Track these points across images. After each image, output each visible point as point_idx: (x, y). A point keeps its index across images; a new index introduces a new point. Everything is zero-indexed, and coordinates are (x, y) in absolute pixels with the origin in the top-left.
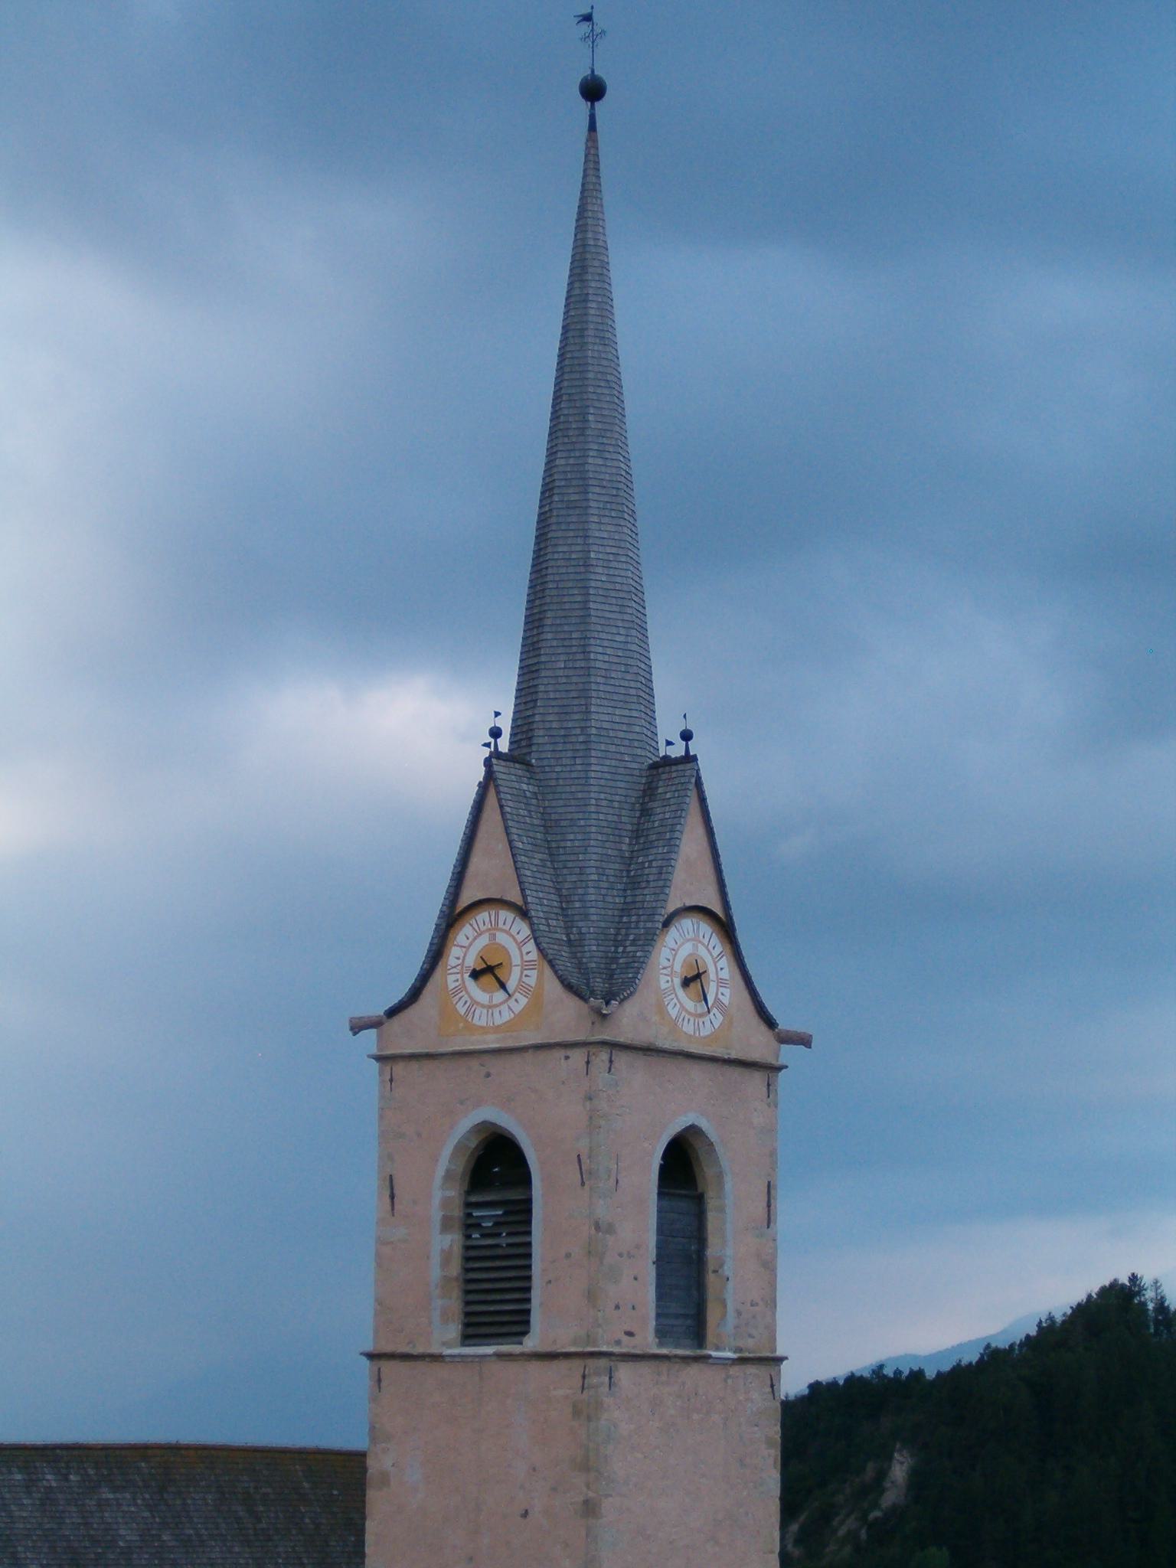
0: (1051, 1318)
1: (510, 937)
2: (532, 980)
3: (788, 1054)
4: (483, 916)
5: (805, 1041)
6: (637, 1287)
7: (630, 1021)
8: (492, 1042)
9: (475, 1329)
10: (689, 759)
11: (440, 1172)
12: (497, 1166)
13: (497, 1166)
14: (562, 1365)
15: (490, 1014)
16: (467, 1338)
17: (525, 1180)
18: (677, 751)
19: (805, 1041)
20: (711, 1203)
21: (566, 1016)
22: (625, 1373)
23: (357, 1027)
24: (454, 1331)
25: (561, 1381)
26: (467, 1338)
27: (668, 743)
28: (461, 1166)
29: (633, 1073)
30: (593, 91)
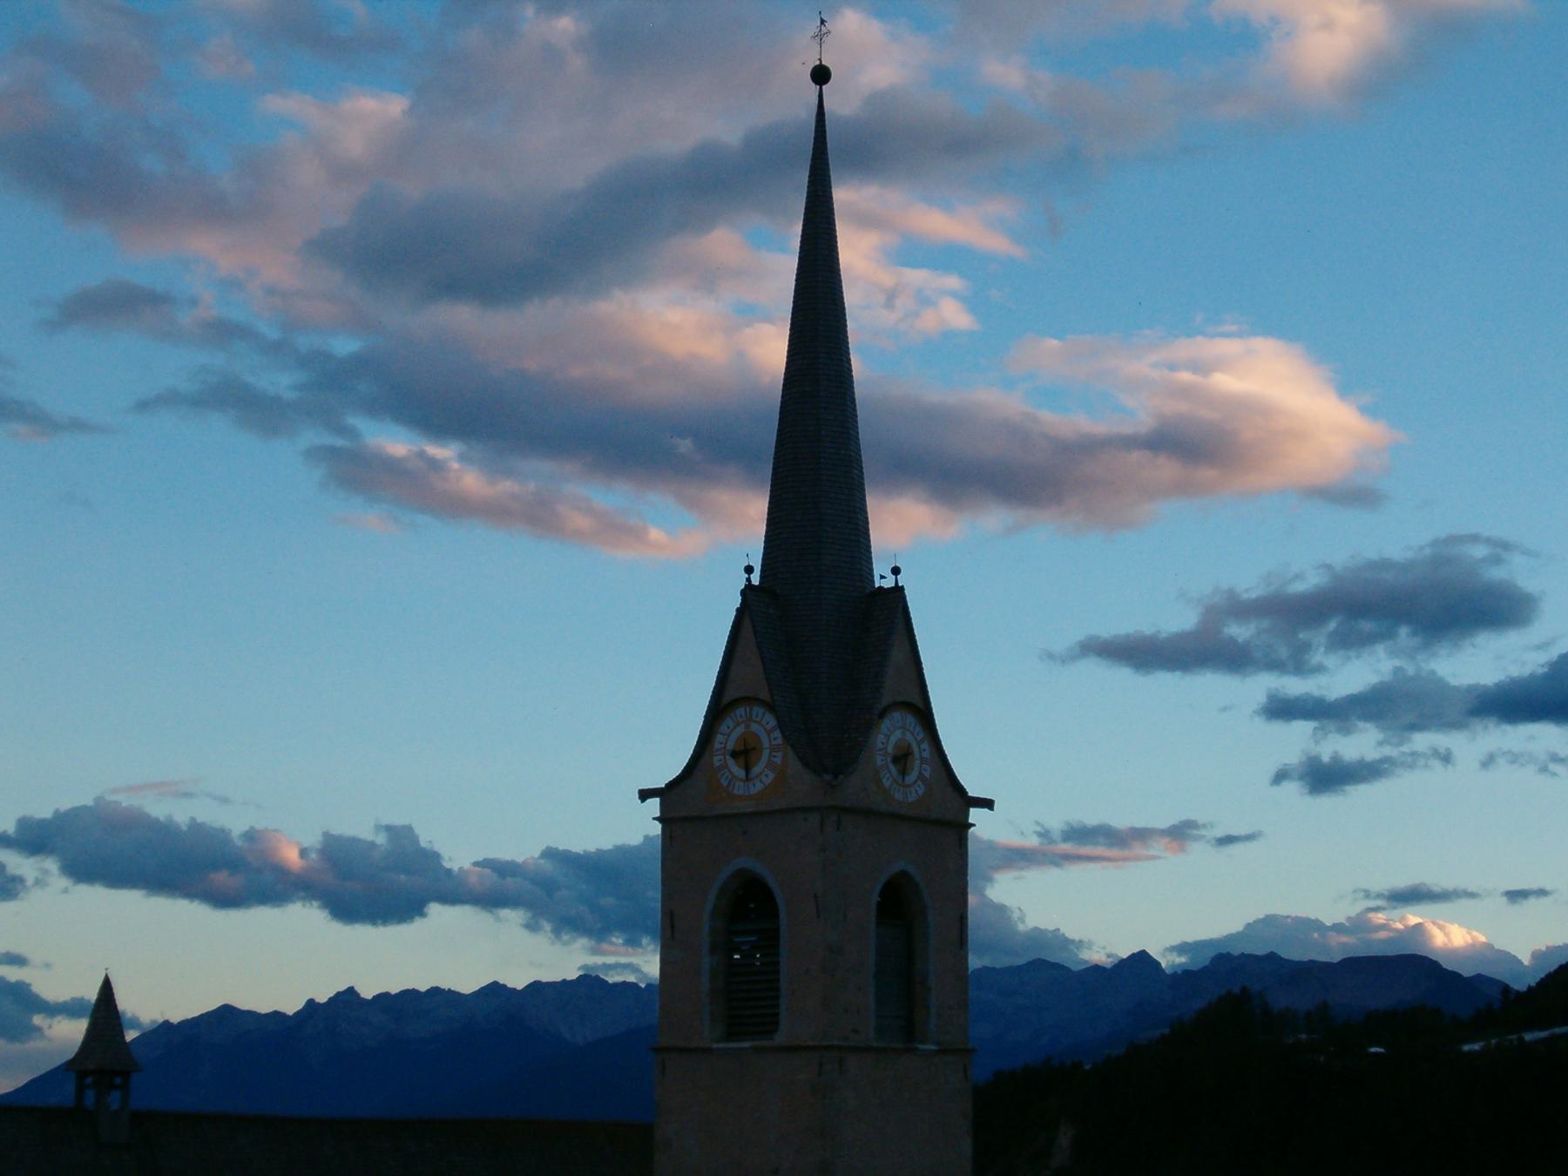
3: (975, 814)
4: (740, 711)
5: (988, 804)
9: (734, 1027)
12: (750, 904)
13: (750, 904)
16: (729, 1037)
17: (773, 913)
19: (988, 804)
23: (645, 795)
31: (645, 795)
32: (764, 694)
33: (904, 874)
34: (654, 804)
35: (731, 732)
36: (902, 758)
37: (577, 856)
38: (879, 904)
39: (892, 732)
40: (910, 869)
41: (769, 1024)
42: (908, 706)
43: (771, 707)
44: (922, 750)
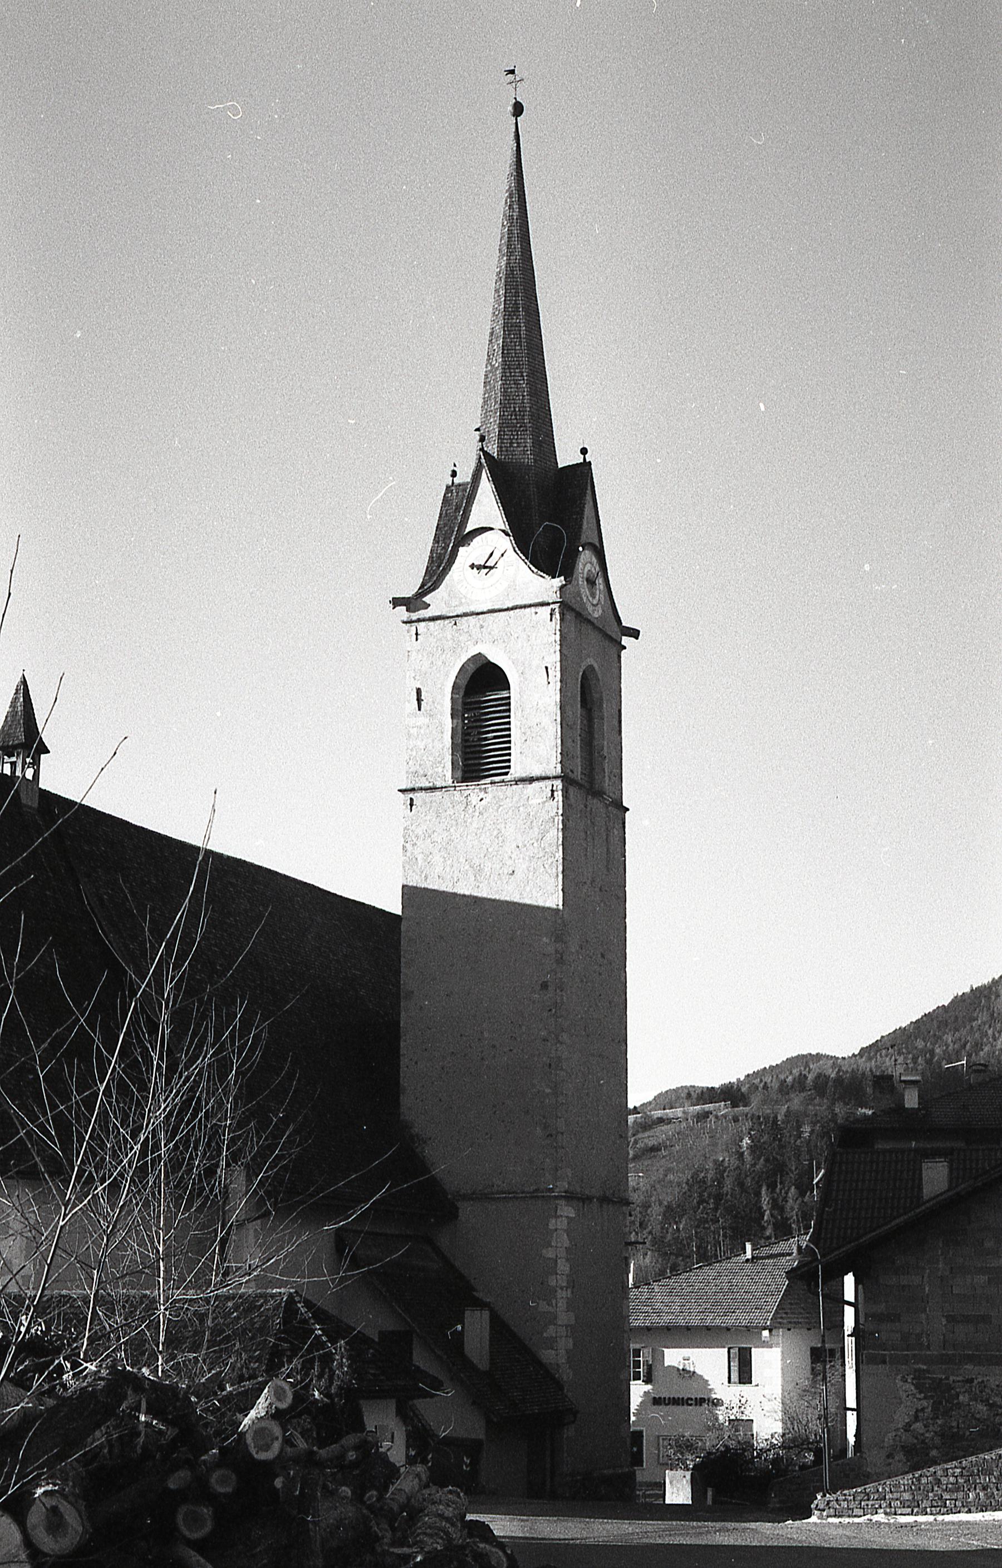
3: (625, 640)
5: (635, 634)
10: (587, 465)
17: (508, 687)
19: (635, 634)
20: (596, 714)
27: (566, 456)
30: (518, 109)
36: (591, 582)
40: (590, 661)
44: (600, 581)
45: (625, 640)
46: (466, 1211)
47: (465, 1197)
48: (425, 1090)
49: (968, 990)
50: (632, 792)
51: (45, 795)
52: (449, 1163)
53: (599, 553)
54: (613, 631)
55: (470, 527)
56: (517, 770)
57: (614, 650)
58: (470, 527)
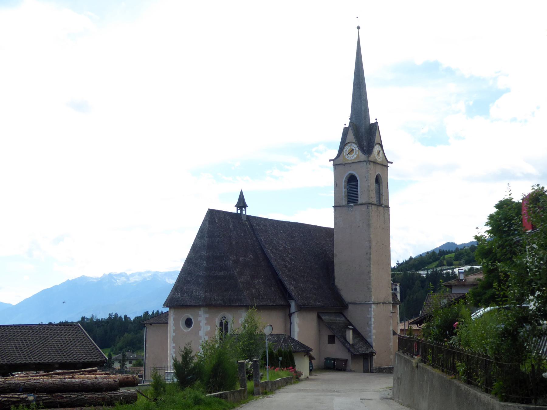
0: (116, 315)
1: (355, 147)
2: (357, 153)
3: (389, 165)
4: (349, 145)
5: (391, 163)
6: (373, 195)
7: (371, 158)
8: (351, 162)
9: (349, 202)
10: (377, 123)
11: (344, 181)
12: (352, 180)
13: (352, 180)
14: (364, 206)
15: (352, 158)
16: (348, 204)
17: (357, 181)
18: (375, 122)
19: (391, 163)
20: (381, 185)
21: (363, 157)
22: (373, 206)
23: (330, 161)
24: (346, 202)
25: (364, 208)
26: (348, 204)
27: (372, 121)
28: (346, 180)
29: (372, 166)
30: (358, 28)
31: (330, 161)
32: (354, 141)
33: (379, 174)
34: (332, 162)
35: (347, 149)
36: (379, 152)
37: (99, 323)
38: (200, 330)
39: (377, 148)
40: (379, 173)
41: (357, 200)
42: (379, 144)
43: (356, 144)
44: (381, 152)
45: (389, 165)
46: (350, 307)
47: (350, 303)
48: (340, 280)
49: (106, 316)
50: (392, 203)
51: (248, 216)
52: (347, 296)
53: (381, 145)
54: (385, 163)
55: (346, 142)
56: (359, 202)
57: (386, 168)
58: (346, 142)
